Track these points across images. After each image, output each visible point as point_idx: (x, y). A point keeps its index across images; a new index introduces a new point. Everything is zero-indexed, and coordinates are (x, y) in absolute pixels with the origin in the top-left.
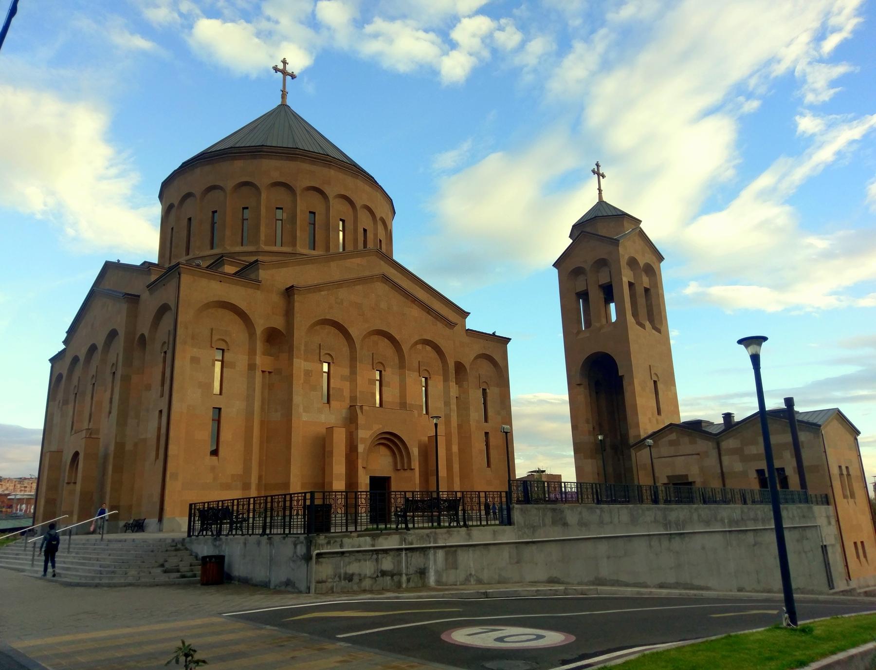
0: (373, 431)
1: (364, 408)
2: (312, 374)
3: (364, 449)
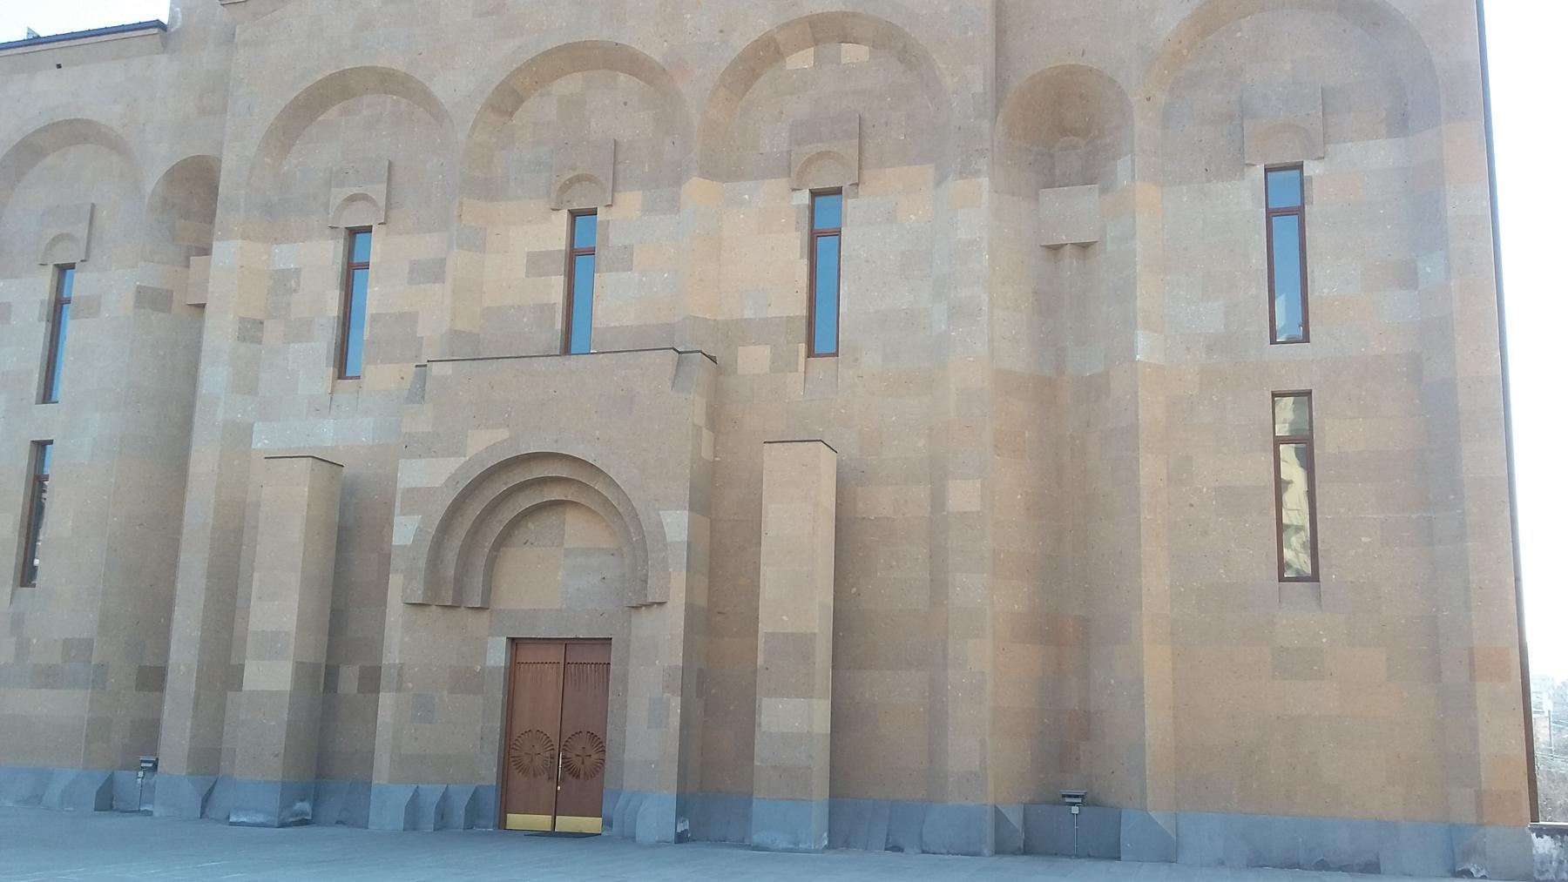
0: (463, 460)
2: (298, 284)
3: (420, 530)
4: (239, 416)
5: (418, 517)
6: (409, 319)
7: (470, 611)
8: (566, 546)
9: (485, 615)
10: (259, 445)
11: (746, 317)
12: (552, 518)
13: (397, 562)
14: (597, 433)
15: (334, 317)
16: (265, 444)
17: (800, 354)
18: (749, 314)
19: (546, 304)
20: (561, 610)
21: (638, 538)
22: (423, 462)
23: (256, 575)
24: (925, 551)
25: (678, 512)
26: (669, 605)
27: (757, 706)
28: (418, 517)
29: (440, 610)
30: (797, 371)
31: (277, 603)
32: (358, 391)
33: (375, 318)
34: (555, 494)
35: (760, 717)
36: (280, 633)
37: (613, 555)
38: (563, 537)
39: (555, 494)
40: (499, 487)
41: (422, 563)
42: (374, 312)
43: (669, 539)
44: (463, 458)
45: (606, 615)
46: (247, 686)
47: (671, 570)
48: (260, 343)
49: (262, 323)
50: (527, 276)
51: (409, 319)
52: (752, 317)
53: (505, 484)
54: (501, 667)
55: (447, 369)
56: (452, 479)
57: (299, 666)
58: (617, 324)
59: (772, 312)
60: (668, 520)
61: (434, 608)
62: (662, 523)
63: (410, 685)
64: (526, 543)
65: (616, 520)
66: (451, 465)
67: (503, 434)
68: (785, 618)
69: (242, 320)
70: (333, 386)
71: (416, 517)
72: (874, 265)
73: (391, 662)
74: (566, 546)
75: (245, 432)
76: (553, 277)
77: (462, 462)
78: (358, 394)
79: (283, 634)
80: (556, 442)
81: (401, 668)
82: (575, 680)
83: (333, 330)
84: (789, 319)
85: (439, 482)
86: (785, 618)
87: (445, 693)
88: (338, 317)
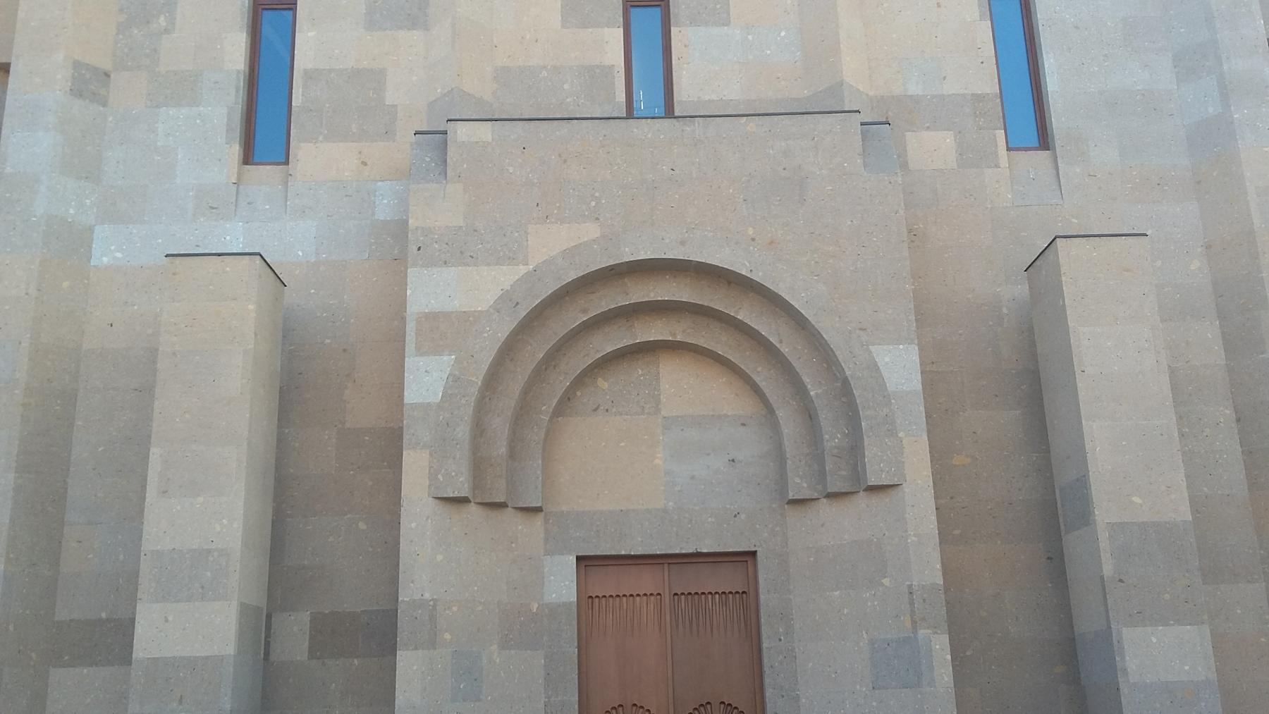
0: (523, 270)
1: (462, 133)
3: (455, 381)
4: (72, 211)
5: (448, 360)
6: (372, 79)
7: (519, 514)
8: (664, 413)
9: (539, 520)
10: (105, 260)
11: (910, 93)
12: (639, 371)
13: (416, 433)
14: (751, 231)
15: (238, 72)
16: (115, 258)
17: (999, 144)
18: (914, 89)
19: (598, 66)
20: (665, 511)
21: (820, 391)
22: (451, 273)
23: (155, 453)
24: (1228, 412)
25: (901, 347)
26: (907, 489)
27: (1115, 643)
28: (448, 360)
29: (513, 510)
30: (997, 166)
31: (201, 499)
32: (286, 183)
33: (309, 75)
34: (655, 331)
35: (1123, 658)
36: (209, 551)
37: (743, 425)
38: (658, 402)
39: (655, 331)
40: (574, 316)
41: (463, 431)
42: (310, 66)
43: (891, 387)
44: (521, 267)
45: (743, 516)
46: (139, 652)
47: (901, 434)
48: (104, 105)
49: (107, 75)
50: (563, 26)
51: (372, 79)
52: (921, 93)
53: (585, 311)
54: (571, 603)
55: (484, 132)
56: (506, 299)
57: (244, 610)
58: (714, 97)
59: (950, 88)
60: (887, 359)
61: (473, 507)
62: (876, 364)
63: (447, 636)
64: (595, 410)
65: (759, 369)
66: (505, 277)
67: (591, 231)
68: (1137, 500)
69: (77, 65)
70: (239, 175)
71: (445, 358)
72: (1086, 33)
73: (417, 597)
74: (664, 413)
75: (81, 241)
76: (606, 29)
77: (522, 273)
78: (286, 187)
79: (216, 554)
80: (683, 243)
81: (435, 606)
82: (691, 622)
83: (237, 91)
84: (978, 98)
85: (484, 299)
86: (1137, 500)
87: (494, 647)
88: (244, 71)
